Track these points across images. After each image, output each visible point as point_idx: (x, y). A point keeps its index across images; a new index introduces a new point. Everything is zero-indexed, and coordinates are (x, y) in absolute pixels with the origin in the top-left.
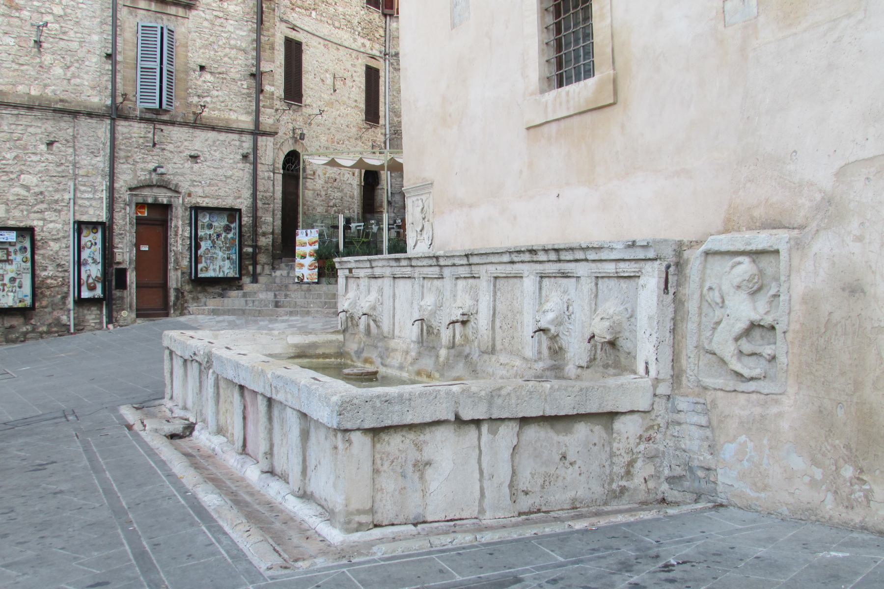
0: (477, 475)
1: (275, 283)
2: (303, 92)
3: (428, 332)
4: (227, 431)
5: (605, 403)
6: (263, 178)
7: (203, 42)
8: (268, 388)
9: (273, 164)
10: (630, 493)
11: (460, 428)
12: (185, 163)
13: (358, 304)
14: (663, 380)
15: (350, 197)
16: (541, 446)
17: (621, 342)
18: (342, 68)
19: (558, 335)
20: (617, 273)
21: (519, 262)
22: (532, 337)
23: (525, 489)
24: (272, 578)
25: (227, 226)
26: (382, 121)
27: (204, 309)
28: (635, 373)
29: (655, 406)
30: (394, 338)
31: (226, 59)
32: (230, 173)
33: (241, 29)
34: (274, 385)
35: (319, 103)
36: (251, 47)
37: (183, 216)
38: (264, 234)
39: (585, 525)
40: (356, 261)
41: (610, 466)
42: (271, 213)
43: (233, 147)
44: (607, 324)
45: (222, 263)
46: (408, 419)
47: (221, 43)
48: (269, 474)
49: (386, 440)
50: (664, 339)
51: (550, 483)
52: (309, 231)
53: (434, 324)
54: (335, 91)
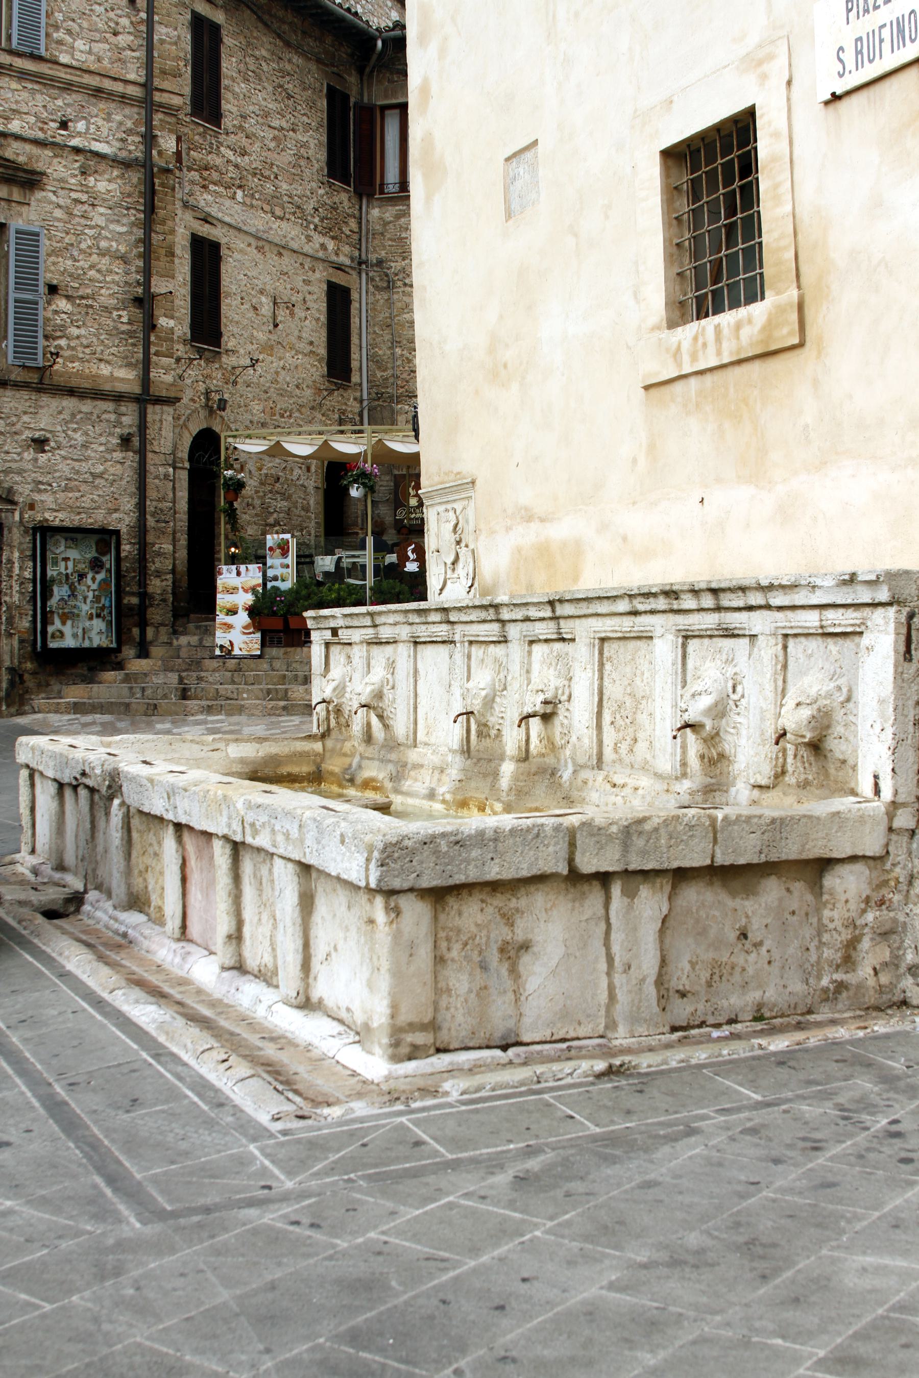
0: (603, 966)
1: (178, 657)
2: (223, 329)
3: (480, 734)
4: (148, 903)
5: (811, 844)
6: (157, 477)
7: (55, 244)
8: (238, 828)
9: (173, 453)
10: (851, 993)
11: (574, 886)
12: (24, 451)
13: (348, 690)
14: (904, 805)
15: (303, 509)
16: (707, 917)
17: (832, 744)
18: (288, 286)
19: (717, 734)
20: (822, 627)
21: (645, 612)
22: (675, 737)
23: (681, 988)
24: (285, 1133)
25: (96, 559)
26: (355, 378)
27: (58, 704)
28: (854, 793)
29: (891, 849)
30: (415, 746)
31: (92, 273)
32: (100, 468)
33: (118, 221)
34: (249, 819)
35: (250, 347)
36: (135, 251)
37: (21, 543)
38: (158, 574)
39: (786, 1043)
40: (345, 616)
41: (818, 948)
42: (171, 537)
43: (104, 424)
44: (806, 713)
45: (87, 624)
46: (493, 872)
47: (83, 246)
48: (234, 973)
49: (455, 907)
50: (904, 737)
51: (721, 977)
52: (243, 568)
53: (492, 720)
54: (276, 326)
